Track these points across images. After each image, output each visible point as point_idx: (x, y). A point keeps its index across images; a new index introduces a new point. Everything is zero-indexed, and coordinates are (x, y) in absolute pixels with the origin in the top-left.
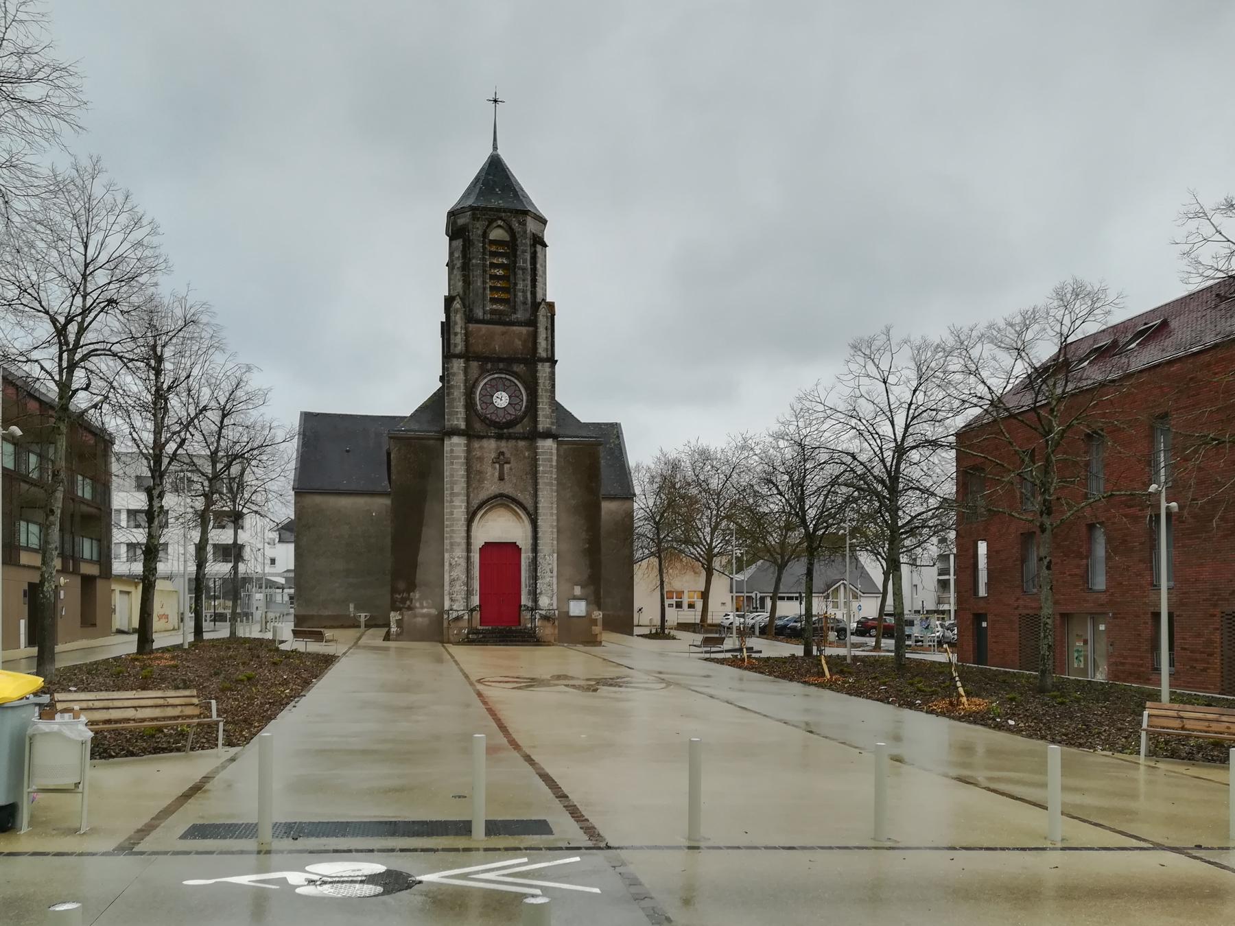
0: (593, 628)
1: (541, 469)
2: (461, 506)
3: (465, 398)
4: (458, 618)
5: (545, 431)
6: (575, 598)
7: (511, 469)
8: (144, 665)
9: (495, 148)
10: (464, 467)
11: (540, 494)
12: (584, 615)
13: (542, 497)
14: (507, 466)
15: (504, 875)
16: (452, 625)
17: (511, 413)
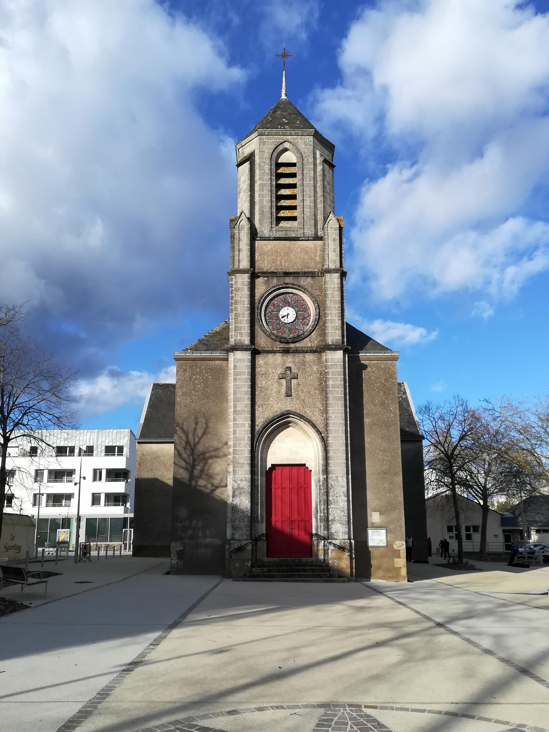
4: (240, 549)
7: (298, 384)
11: (330, 409)
14: (294, 382)
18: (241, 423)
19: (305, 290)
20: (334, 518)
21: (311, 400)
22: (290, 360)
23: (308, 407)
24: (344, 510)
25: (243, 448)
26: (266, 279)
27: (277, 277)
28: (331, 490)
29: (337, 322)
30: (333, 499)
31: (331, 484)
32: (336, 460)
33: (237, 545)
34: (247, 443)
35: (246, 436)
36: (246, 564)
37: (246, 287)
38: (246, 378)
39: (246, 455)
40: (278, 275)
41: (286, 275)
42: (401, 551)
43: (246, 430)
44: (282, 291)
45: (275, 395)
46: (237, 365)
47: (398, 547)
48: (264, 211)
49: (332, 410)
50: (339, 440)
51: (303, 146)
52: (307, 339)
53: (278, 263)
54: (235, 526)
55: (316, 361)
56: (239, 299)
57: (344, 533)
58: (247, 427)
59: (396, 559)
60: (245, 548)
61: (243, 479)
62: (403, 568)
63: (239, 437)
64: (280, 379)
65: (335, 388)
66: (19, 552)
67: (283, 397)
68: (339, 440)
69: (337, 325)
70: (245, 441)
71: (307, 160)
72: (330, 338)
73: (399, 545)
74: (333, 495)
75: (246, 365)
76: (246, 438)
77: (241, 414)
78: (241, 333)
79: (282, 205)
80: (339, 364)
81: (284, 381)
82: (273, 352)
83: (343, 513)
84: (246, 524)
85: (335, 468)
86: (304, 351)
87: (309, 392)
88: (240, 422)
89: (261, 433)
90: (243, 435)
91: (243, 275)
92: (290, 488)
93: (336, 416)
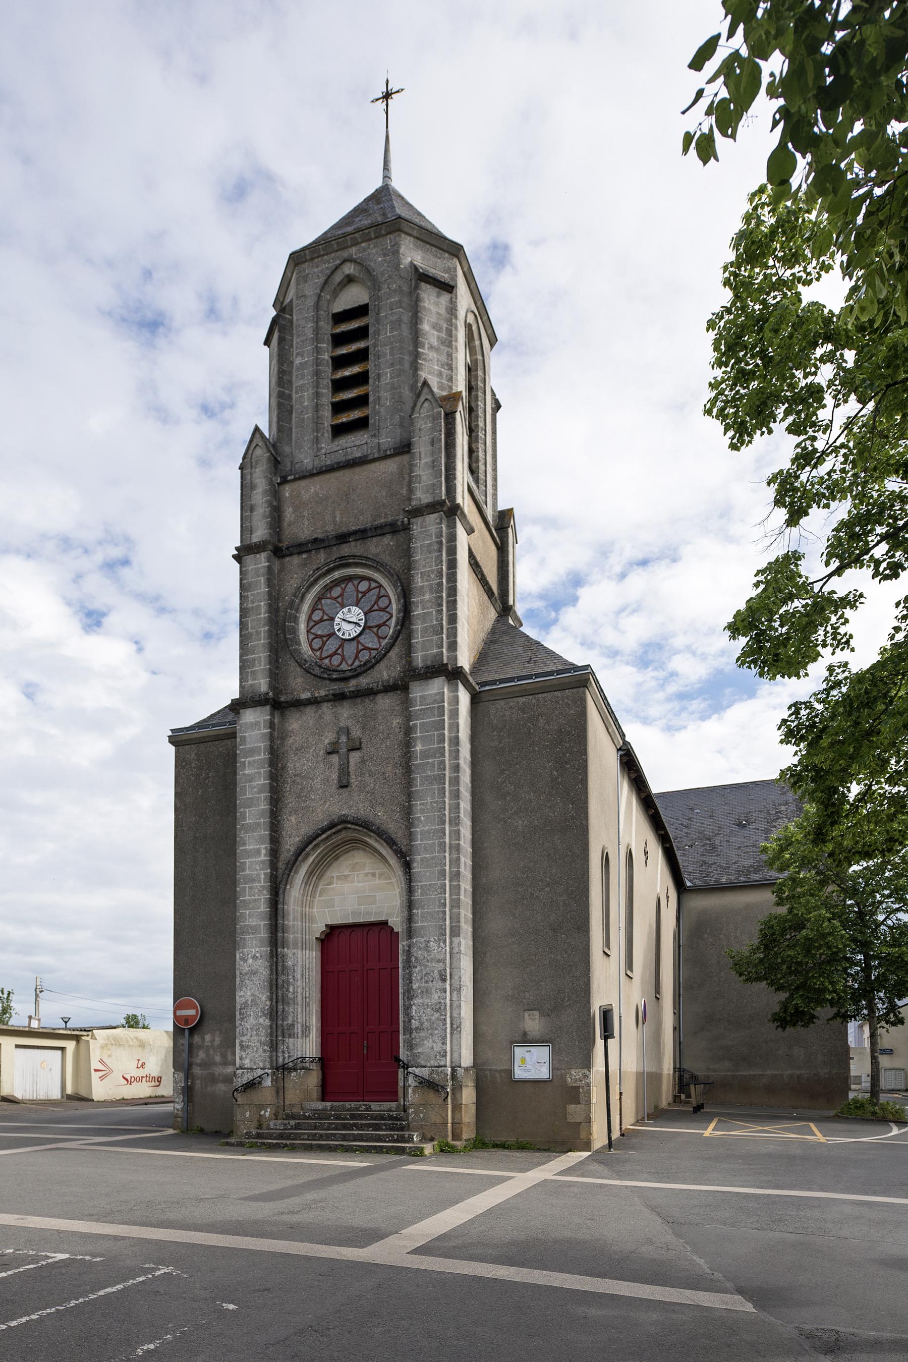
0: (572, 1107)
1: (419, 748)
2: (258, 852)
3: (270, 631)
4: (251, 1086)
5: (429, 663)
6: (526, 1040)
7: (363, 761)
8: (772, 980)
9: (386, 177)
10: (265, 770)
11: (418, 804)
12: (547, 1076)
13: (422, 811)
14: (355, 757)
15: (774, 1129)
16: (241, 1099)
17: (370, 645)
18: (254, 849)
19: (377, 565)
20: (422, 1025)
21: (387, 790)
22: (346, 713)
23: (380, 804)
24: (440, 1008)
25: (257, 897)
26: (304, 556)
27: (325, 547)
28: (417, 970)
29: (434, 618)
30: (419, 987)
31: (416, 958)
32: (426, 907)
33: (247, 1077)
34: (263, 886)
35: (262, 872)
36: (262, 1113)
37: (262, 579)
38: (261, 759)
39: (262, 910)
40: (326, 544)
41: (342, 541)
42: (581, 1090)
43: (263, 862)
44: (337, 574)
45: (319, 787)
46: (245, 736)
47: (576, 1080)
48: (304, 418)
49: (420, 804)
50: (434, 865)
51: (380, 259)
52: (382, 665)
53: (328, 518)
54: (244, 1043)
55: (397, 708)
56: (250, 605)
57: (440, 1053)
58: (262, 855)
59: (571, 1106)
60: (260, 1083)
61: (257, 955)
62: (583, 1124)
63: (250, 875)
64: (329, 753)
65: (428, 757)
66: (158, 1086)
67: (334, 789)
68: (434, 865)
69: (435, 623)
70: (260, 882)
71: (388, 287)
72: (420, 654)
73: (578, 1077)
74: (419, 978)
75: (262, 733)
76: (262, 876)
77: (253, 831)
78: (253, 673)
79: (342, 400)
80: (436, 705)
81: (335, 759)
82: (314, 702)
83: (438, 1014)
84: (263, 1039)
85: (426, 924)
86: (370, 693)
87: (384, 773)
88: (251, 847)
89: (293, 864)
90: (257, 870)
91: (258, 556)
92: (365, 970)
93: (427, 818)
